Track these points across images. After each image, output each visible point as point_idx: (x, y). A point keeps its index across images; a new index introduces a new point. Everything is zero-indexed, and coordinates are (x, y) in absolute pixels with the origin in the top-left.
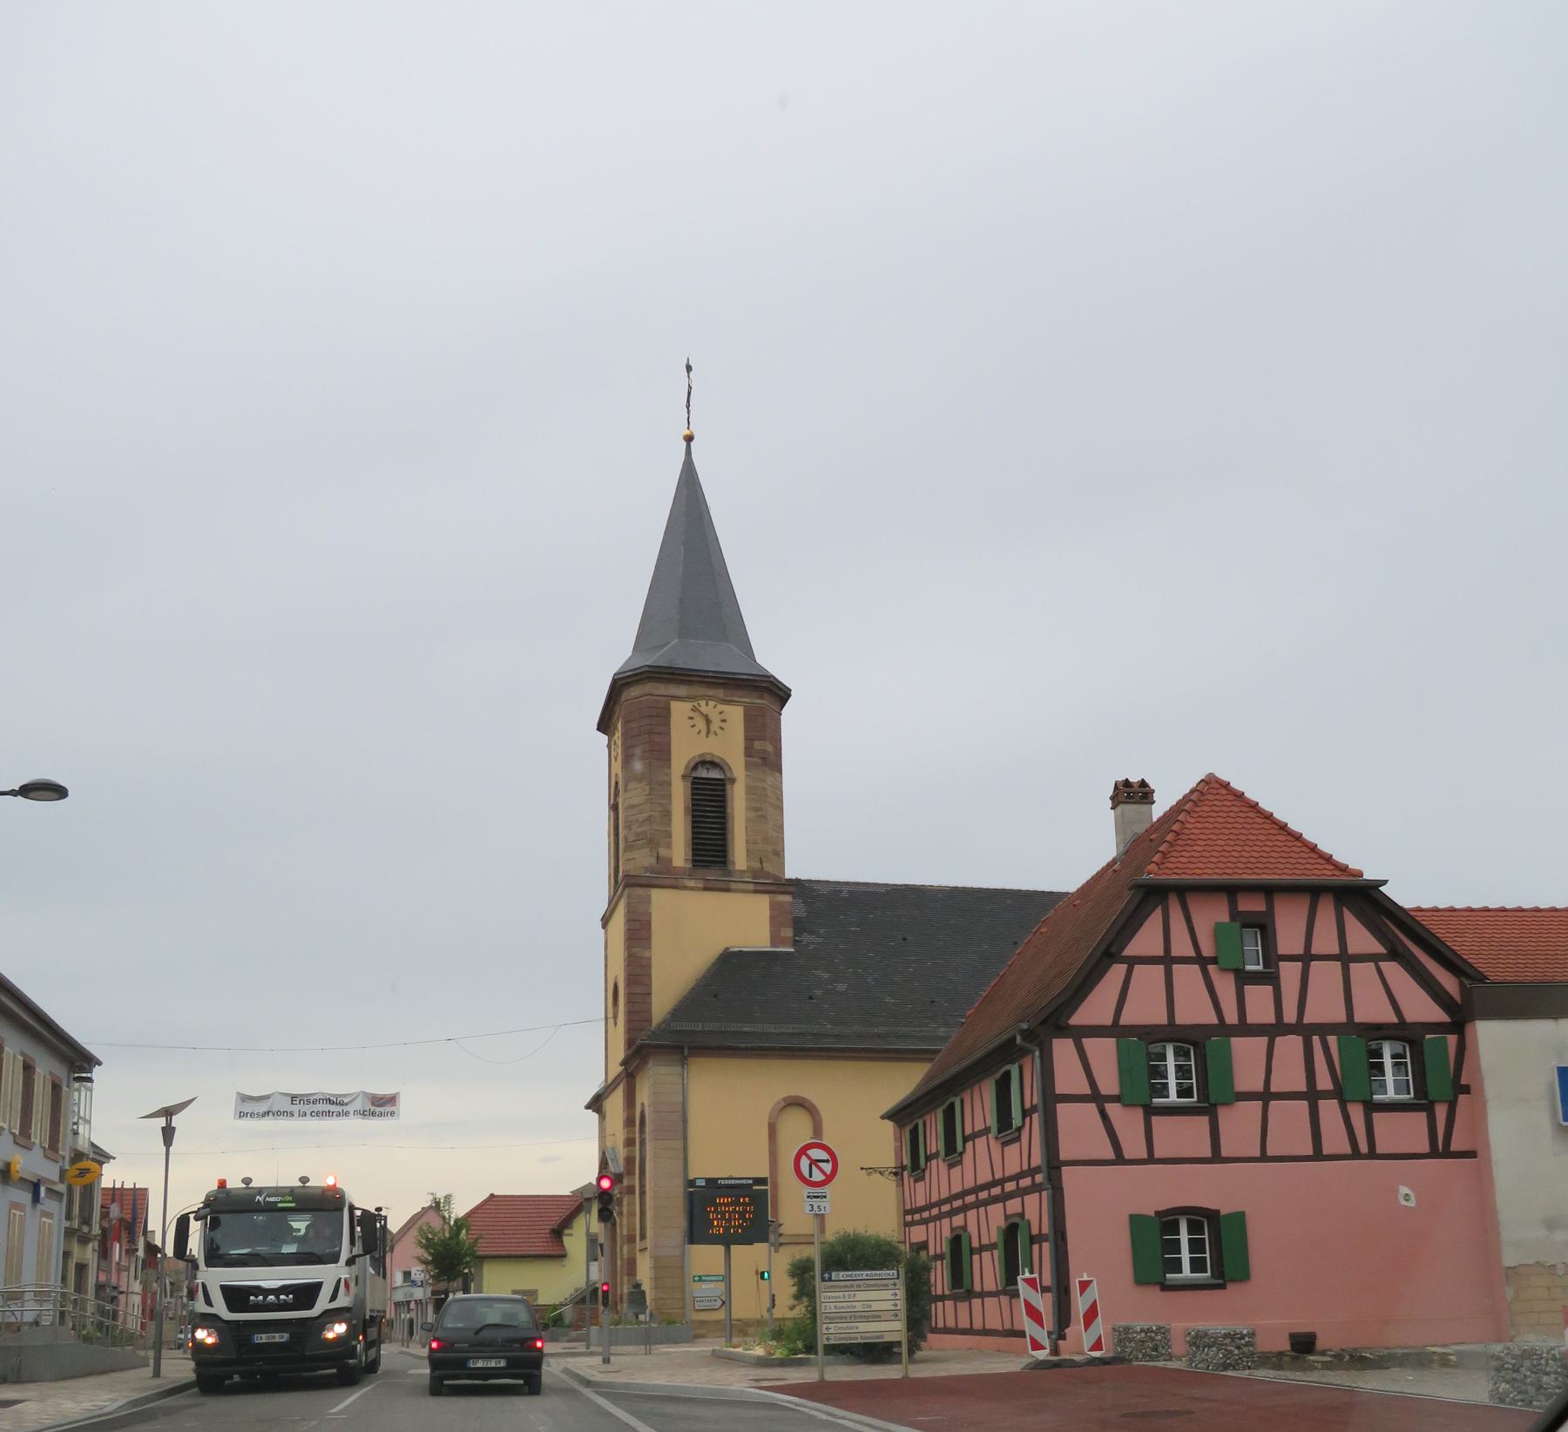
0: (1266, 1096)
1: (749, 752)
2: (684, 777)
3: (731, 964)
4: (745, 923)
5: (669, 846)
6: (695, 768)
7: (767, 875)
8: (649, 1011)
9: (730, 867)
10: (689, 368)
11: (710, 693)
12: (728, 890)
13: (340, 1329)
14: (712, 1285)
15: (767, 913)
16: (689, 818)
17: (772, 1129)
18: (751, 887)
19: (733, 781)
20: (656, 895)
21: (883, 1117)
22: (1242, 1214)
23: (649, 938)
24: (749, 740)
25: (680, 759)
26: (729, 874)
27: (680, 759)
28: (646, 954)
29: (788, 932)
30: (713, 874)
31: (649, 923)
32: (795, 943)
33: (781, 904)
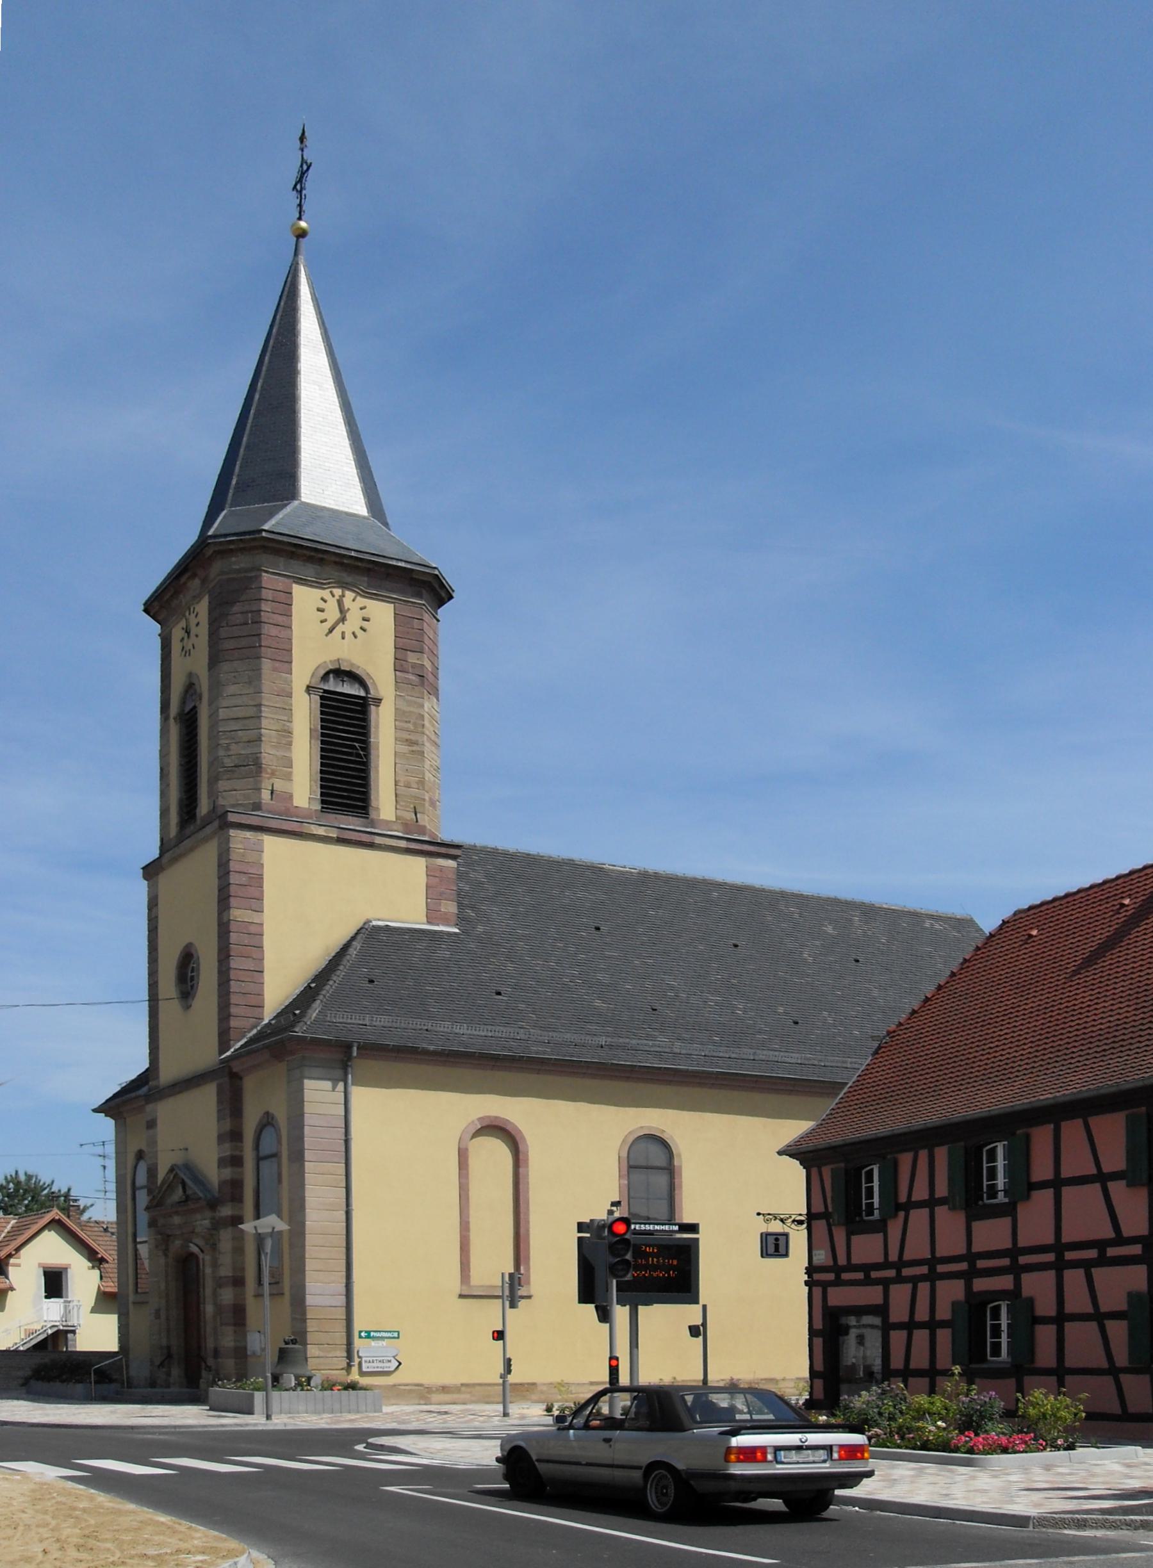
0: (1057, 1183)
1: (400, 665)
2: (309, 689)
3: (373, 944)
4: (395, 892)
5: (288, 777)
6: (325, 677)
7: (423, 830)
8: (261, 994)
9: (373, 815)
10: (302, 139)
11: (349, 579)
12: (371, 846)
13: (939, 1423)
14: (384, 1343)
15: (423, 879)
16: (318, 745)
17: (463, 1157)
18: (403, 844)
19: (378, 701)
20: (268, 840)
21: (780, 1153)
22: (46, 1297)
23: (260, 899)
24: (400, 650)
25: (304, 667)
26: (372, 824)
27: (304, 667)
28: (255, 918)
29: (450, 908)
30: (352, 822)
31: (260, 877)
32: (461, 920)
33: (441, 869)
